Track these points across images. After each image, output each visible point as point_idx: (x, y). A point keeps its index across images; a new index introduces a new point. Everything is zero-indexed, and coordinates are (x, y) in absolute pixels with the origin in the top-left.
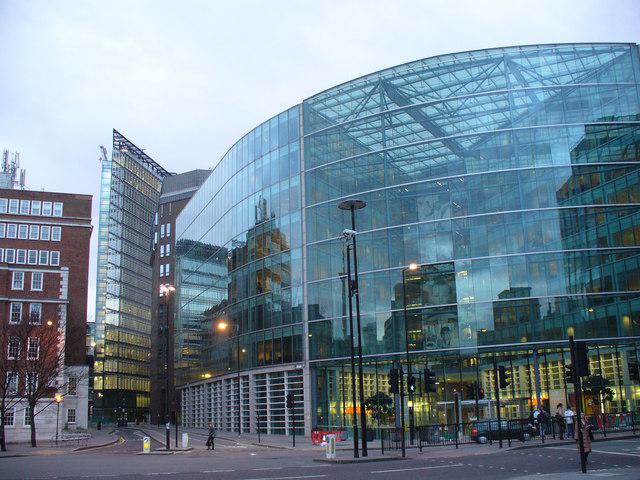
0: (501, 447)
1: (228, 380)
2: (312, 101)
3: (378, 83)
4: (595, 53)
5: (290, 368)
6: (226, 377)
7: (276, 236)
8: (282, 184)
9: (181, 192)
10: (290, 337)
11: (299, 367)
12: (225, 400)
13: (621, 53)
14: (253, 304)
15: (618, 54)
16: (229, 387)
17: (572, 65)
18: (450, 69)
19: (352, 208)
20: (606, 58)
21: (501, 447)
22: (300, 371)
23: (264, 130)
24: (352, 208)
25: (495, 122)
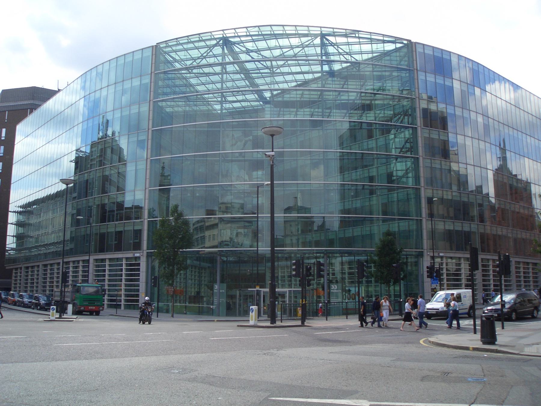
0: (157, 317)
1: (46, 266)
2: (164, 45)
3: (220, 39)
4: (371, 41)
5: (130, 255)
6: (26, 265)
7: (117, 151)
8: (132, 107)
9: (19, 103)
10: (121, 232)
11: (137, 255)
12: (23, 281)
13: (401, 45)
14: (97, 202)
15: (399, 45)
16: (27, 272)
17: (367, 47)
18: (276, 36)
19: (272, 136)
20: (390, 47)
21: (157, 317)
22: (138, 258)
23: (119, 63)
24: (272, 136)
25: (296, 81)
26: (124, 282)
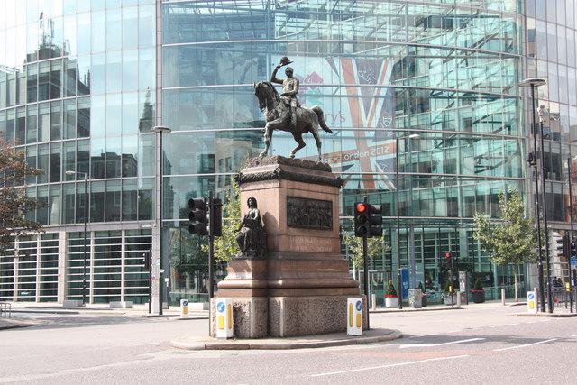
11: (148, 226)
22: (150, 230)
26: (123, 266)
